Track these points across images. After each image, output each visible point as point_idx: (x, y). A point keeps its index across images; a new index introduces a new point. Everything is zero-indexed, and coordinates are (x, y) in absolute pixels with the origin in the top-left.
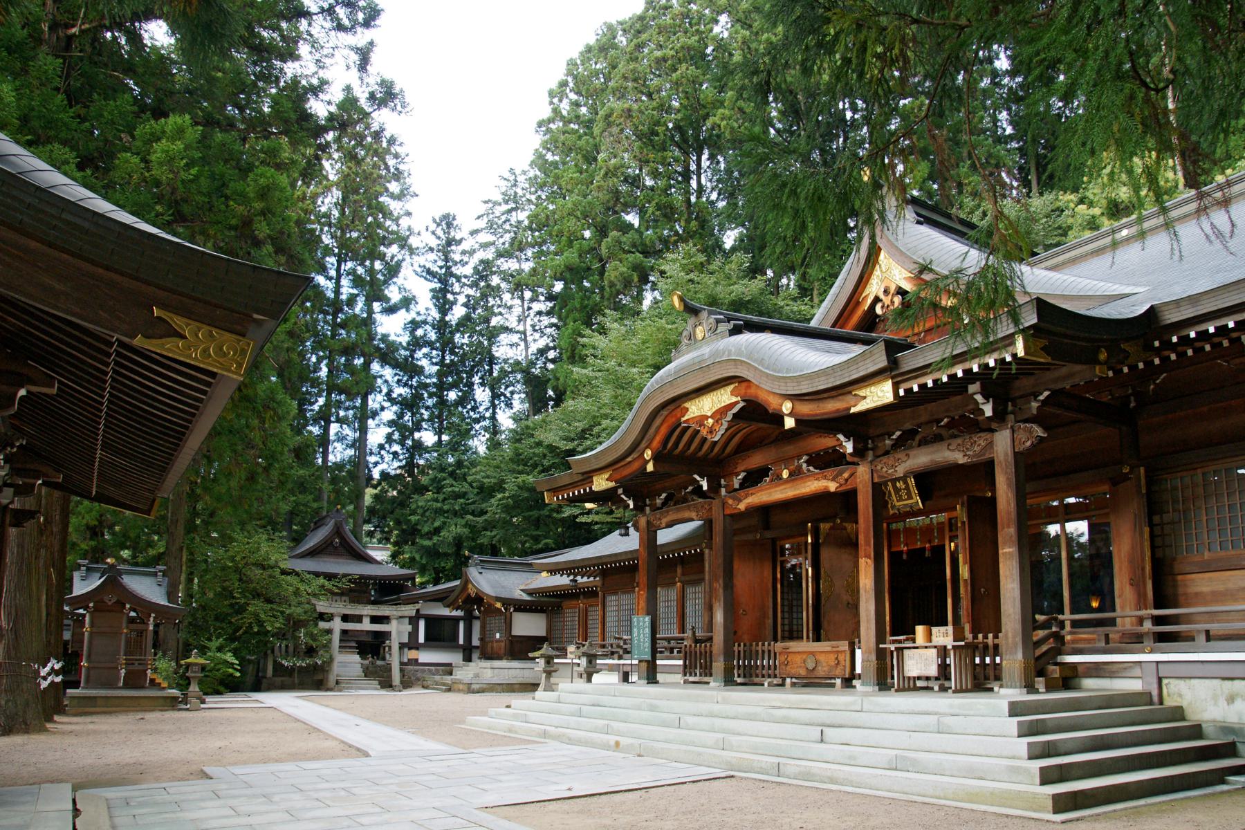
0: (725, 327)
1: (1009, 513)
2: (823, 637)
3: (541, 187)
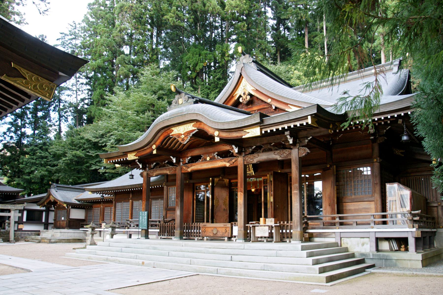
0: (191, 100)
1: (296, 178)
2: (214, 221)
3: (85, 31)
